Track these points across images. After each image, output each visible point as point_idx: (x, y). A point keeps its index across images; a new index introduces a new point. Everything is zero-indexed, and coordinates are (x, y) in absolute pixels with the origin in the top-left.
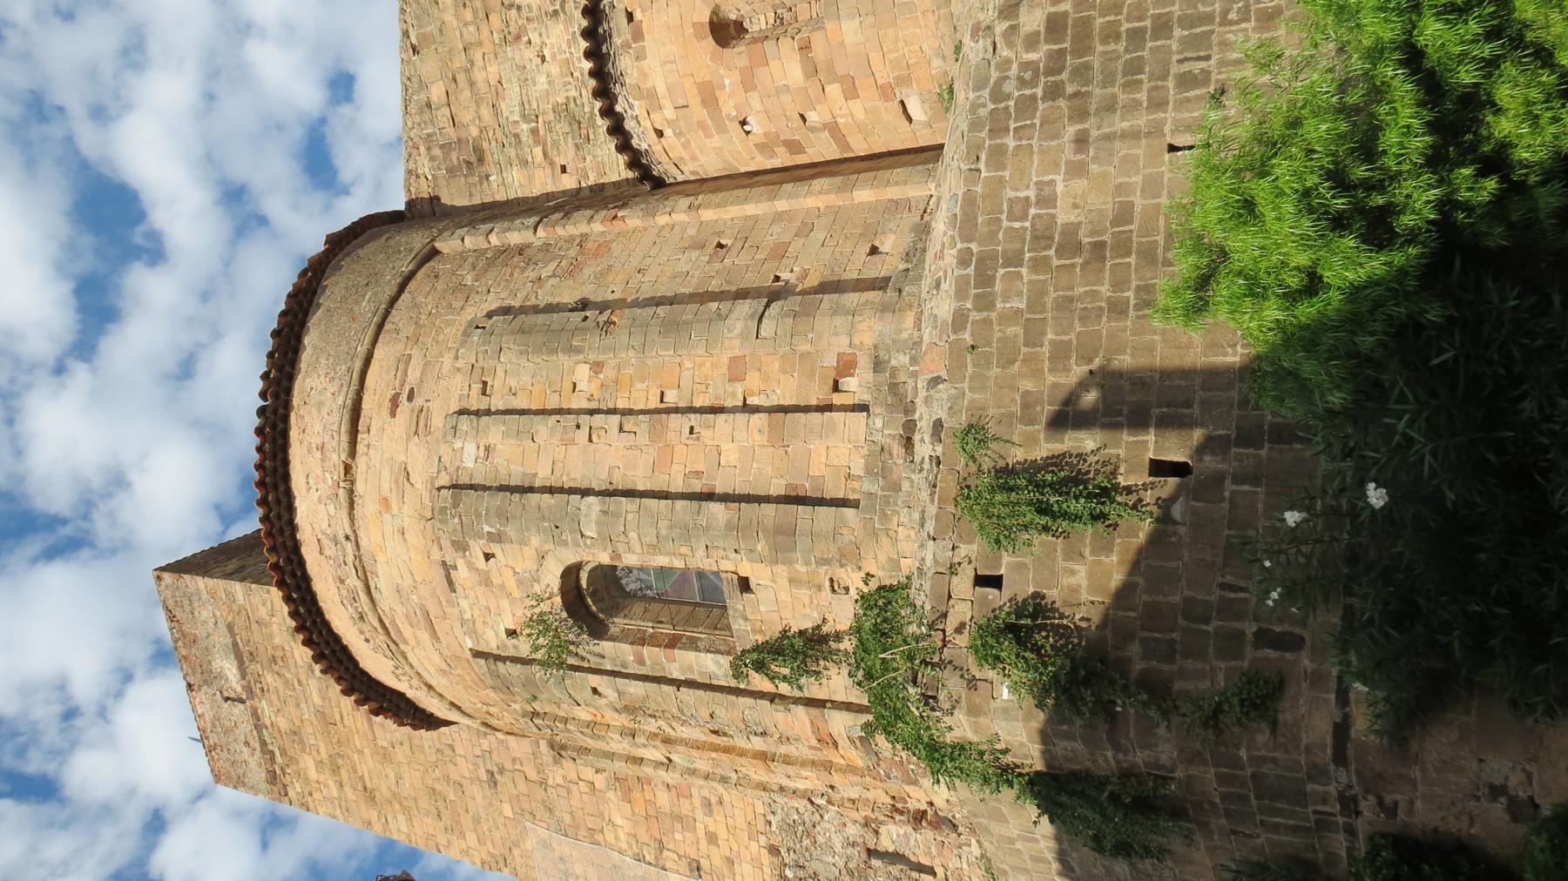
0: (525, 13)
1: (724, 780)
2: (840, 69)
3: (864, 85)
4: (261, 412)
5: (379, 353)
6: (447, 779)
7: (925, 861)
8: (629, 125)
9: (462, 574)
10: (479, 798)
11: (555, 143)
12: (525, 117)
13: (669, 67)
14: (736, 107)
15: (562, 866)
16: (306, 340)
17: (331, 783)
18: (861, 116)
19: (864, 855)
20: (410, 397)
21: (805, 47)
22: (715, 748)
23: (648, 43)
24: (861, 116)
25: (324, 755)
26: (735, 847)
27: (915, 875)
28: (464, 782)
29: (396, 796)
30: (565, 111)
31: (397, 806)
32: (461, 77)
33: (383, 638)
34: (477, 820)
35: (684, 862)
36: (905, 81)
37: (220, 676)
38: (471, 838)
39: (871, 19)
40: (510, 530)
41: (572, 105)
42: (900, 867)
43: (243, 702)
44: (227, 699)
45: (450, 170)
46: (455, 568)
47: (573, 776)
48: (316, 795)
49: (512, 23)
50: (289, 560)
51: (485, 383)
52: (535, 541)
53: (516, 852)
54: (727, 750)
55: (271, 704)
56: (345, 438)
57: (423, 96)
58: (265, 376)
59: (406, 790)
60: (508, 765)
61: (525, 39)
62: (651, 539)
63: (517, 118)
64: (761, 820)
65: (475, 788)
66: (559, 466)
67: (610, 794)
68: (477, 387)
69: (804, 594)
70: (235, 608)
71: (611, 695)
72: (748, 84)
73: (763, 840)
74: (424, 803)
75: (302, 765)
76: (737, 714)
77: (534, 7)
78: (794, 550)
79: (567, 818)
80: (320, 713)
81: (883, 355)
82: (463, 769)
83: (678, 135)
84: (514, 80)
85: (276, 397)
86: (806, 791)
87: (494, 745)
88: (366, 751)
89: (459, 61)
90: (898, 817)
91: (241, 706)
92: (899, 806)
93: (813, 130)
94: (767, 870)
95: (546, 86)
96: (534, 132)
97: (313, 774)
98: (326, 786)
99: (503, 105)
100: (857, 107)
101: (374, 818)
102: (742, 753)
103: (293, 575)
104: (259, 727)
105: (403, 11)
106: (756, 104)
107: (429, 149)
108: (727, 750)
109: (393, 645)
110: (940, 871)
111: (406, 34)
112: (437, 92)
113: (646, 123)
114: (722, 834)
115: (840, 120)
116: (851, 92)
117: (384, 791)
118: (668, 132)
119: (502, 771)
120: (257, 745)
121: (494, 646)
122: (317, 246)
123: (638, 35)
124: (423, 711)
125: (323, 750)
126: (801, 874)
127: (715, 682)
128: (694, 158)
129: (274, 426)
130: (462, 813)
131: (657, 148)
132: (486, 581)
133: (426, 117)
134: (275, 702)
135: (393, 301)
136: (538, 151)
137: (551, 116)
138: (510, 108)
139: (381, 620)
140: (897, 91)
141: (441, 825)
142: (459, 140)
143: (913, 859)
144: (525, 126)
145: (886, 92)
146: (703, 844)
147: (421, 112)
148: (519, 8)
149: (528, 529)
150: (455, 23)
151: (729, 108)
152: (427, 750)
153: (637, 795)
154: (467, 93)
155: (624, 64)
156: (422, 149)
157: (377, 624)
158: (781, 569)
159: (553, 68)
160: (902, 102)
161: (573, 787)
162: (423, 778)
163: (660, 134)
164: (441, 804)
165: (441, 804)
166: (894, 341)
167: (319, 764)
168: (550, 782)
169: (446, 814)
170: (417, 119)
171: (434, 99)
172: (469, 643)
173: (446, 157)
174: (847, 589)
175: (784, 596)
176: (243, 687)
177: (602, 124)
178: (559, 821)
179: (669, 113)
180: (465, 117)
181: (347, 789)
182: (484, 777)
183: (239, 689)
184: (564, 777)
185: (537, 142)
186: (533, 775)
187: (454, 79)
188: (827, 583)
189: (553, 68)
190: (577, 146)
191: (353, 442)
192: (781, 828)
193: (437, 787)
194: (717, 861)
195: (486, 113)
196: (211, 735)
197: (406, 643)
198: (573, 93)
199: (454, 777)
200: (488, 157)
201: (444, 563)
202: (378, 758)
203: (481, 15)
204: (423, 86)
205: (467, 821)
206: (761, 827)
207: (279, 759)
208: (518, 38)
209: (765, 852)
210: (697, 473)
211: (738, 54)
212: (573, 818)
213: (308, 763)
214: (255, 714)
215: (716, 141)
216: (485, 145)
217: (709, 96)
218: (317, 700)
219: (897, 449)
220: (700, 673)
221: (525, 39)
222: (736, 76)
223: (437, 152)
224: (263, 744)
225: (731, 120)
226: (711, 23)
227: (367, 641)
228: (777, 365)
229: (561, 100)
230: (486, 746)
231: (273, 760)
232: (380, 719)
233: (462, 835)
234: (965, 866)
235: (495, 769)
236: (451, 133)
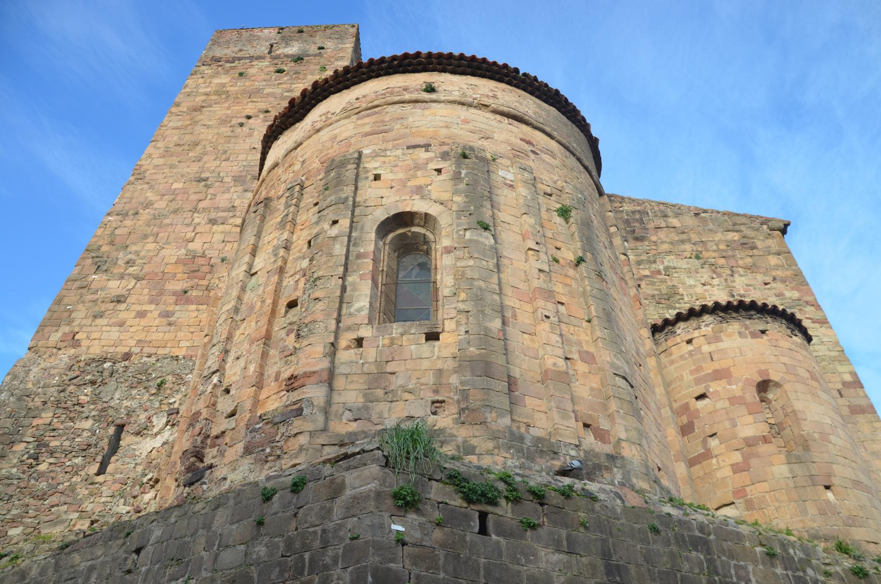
0: (729, 278)
1: (236, 310)
2: (754, 462)
3: (742, 478)
4: (516, 70)
5: (553, 143)
6: (205, 154)
7: (110, 468)
8: (693, 323)
9: (422, 155)
10: (189, 170)
11: (653, 284)
12: (667, 268)
13: (738, 351)
14: (716, 392)
15: (131, 212)
16: (551, 108)
17: (209, 90)
18: (719, 475)
19: (119, 422)
20: (533, 152)
21: (765, 440)
22: (275, 304)
23: (750, 340)
24: (719, 475)
25: (228, 89)
26: (132, 329)
27: (99, 458)
28: (201, 164)
29: (196, 122)
30: (672, 295)
31: (188, 123)
32: (685, 236)
33: (364, 106)
34: (172, 166)
35: (124, 292)
36: (750, 505)
37: (287, 45)
38: (161, 161)
39: (792, 485)
40: (462, 186)
41: (679, 297)
42: (106, 448)
43: (270, 53)
44: (272, 46)
45: (627, 222)
46: (427, 151)
47: (198, 229)
48: (201, 80)
49: (722, 270)
50: (420, 63)
51: (551, 195)
52: (458, 199)
53: (146, 186)
54: (273, 312)
55: (267, 67)
56: (506, 109)
57: (670, 214)
58: (535, 79)
59: (198, 129)
60: (211, 191)
61: (714, 276)
62: (469, 274)
63: (666, 263)
64: (153, 351)
65: (196, 169)
66: (508, 227)
67: (183, 251)
68: (548, 190)
69: (430, 379)
70: (332, 60)
71: (334, 231)
72: (733, 400)
73: (136, 350)
74: (188, 138)
75: (223, 76)
76: (319, 316)
77: (734, 284)
78: (473, 375)
79: (167, 221)
80: (258, 91)
81: (619, 463)
82: (210, 163)
83: (690, 353)
84: (689, 266)
85: (523, 81)
86: (224, 369)
87: (226, 185)
88: (229, 112)
89: (695, 238)
90: (199, 439)
91: (267, 51)
92: (209, 441)
93: (704, 442)
94: (111, 350)
95: (688, 283)
96: (659, 272)
97: (216, 81)
98: (207, 87)
99: (672, 257)
100: (727, 472)
101: (181, 109)
102: (270, 323)
103: (410, 65)
104: (251, 58)
105: (718, 212)
106: (720, 405)
107: (639, 211)
108: (273, 312)
109: (349, 112)
110: (101, 479)
111: (705, 211)
112: (675, 222)
113: (696, 334)
114: (144, 322)
115: (714, 461)
116: (736, 469)
117: (199, 117)
118: (690, 347)
119: (207, 187)
120: (240, 55)
121: (366, 165)
122: (595, 132)
123: (754, 335)
124: (281, 133)
125: (232, 89)
126: (106, 374)
127: (345, 305)
128: (672, 362)
129: (507, 75)
130: (179, 159)
131: (678, 339)
132: (417, 167)
133: (659, 213)
134: (268, 69)
135: (579, 160)
136: (647, 273)
137: (670, 283)
138: (670, 261)
139: (377, 106)
140: (741, 500)
141: (172, 145)
142: (647, 229)
143: (113, 459)
144: (661, 267)
145: (740, 492)
146: (139, 308)
147: (662, 212)
148: (732, 275)
149: (466, 196)
150: (716, 239)
151: (714, 387)
152: (226, 145)
153: (181, 268)
154: (676, 238)
155: (734, 326)
156: (638, 208)
157: (375, 103)
158: (450, 364)
159: (699, 289)
160: (733, 503)
161: (191, 228)
162: (206, 140)
163: (689, 342)
164: (186, 147)
165: (186, 147)
166: (629, 472)
167: (223, 85)
168: (196, 215)
169: (180, 149)
170: (656, 208)
171: (670, 220)
172: (366, 151)
173: (636, 220)
174: (434, 413)
175: (425, 364)
176: (280, 55)
177: (671, 314)
178: (166, 216)
179: (706, 349)
180: (662, 235)
181: (204, 97)
182: (204, 175)
183: (278, 52)
184: (199, 224)
185: (652, 273)
186: (202, 205)
187: (683, 233)
188: (440, 398)
189: (699, 289)
190: (653, 296)
191: (502, 114)
192: (145, 363)
193: (199, 147)
194: (123, 316)
195: (665, 247)
196: (248, 34)
197: (358, 119)
198: (686, 299)
199: (205, 158)
200: (638, 244)
201: (430, 145)
202: (224, 117)
203: (724, 254)
204: (677, 215)
205: (174, 160)
206: (147, 350)
207: (228, 65)
208: (714, 272)
209: (126, 350)
210: (516, 316)
211: (752, 395)
212: (168, 225)
213: (224, 79)
214: (260, 58)
215: (688, 377)
216: (647, 243)
217: (720, 375)
218: (267, 90)
219: (557, 464)
220: (352, 296)
221: (714, 276)
222: (739, 393)
223: (637, 216)
224: (240, 59)
225: (707, 387)
226: (770, 381)
227: (357, 99)
228: (595, 385)
229: (681, 291)
230: (226, 179)
231: (228, 62)
232: (286, 104)
233: (162, 156)
234: (103, 499)
235: (209, 183)
236: (651, 226)
